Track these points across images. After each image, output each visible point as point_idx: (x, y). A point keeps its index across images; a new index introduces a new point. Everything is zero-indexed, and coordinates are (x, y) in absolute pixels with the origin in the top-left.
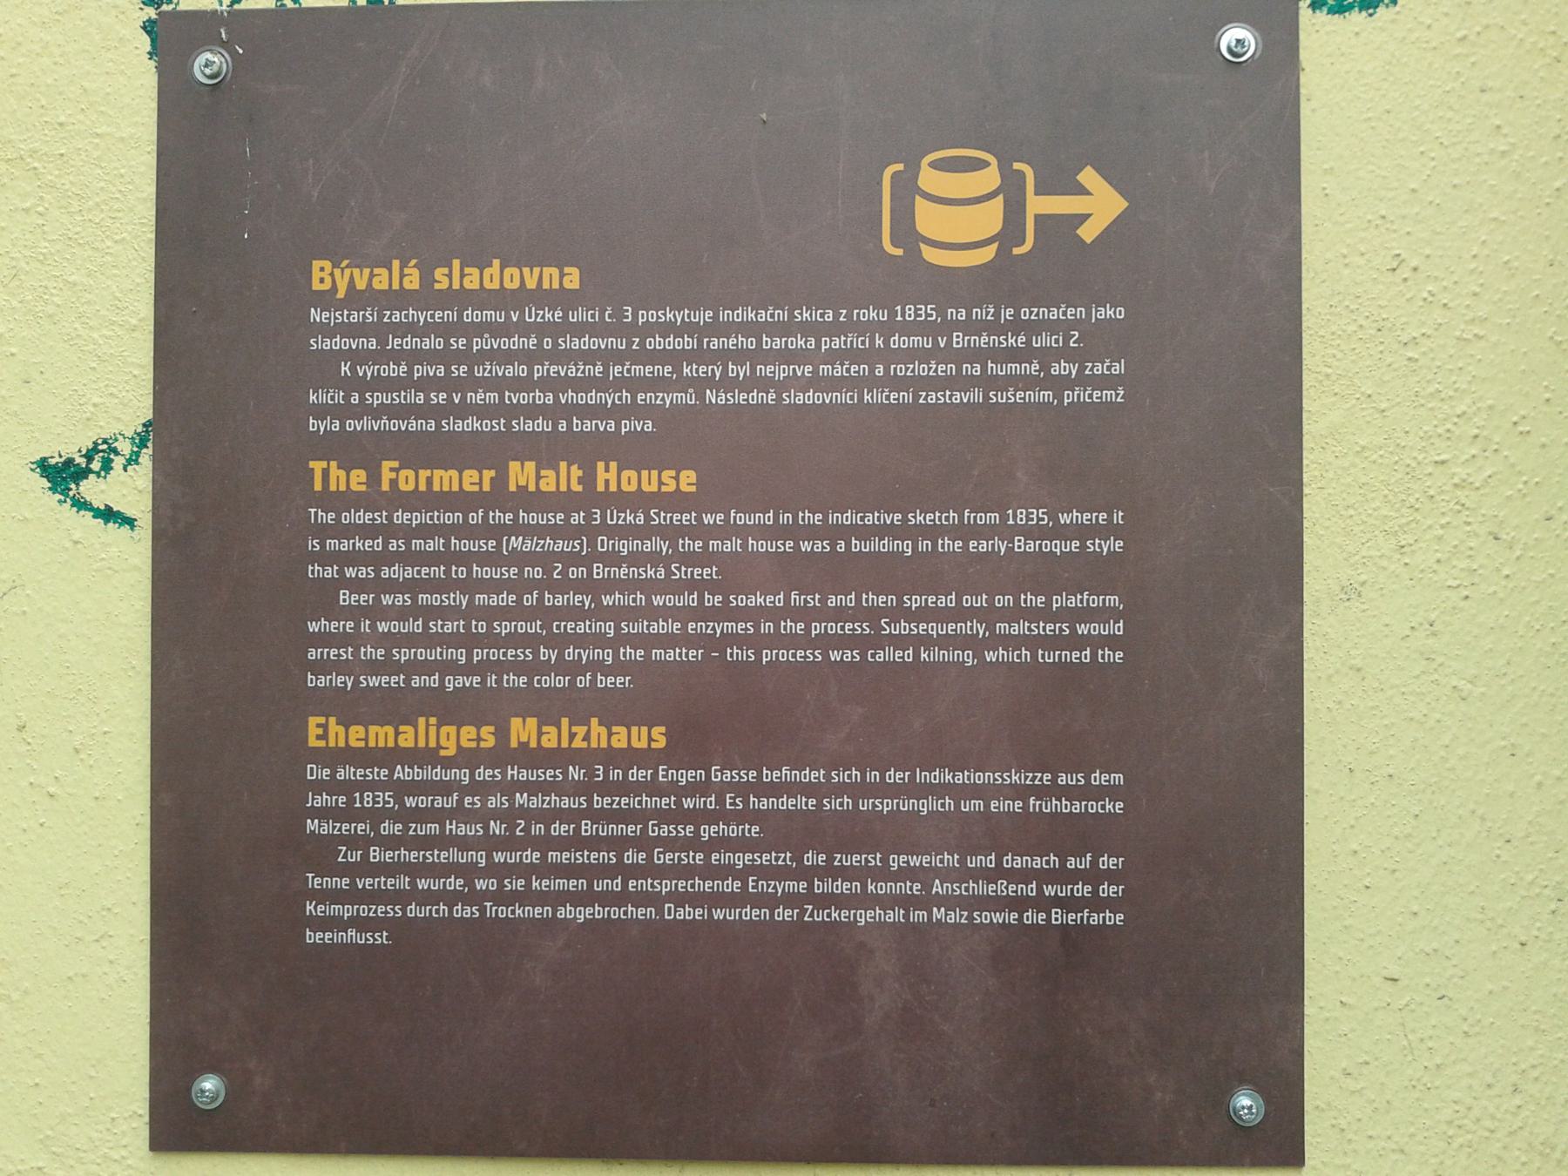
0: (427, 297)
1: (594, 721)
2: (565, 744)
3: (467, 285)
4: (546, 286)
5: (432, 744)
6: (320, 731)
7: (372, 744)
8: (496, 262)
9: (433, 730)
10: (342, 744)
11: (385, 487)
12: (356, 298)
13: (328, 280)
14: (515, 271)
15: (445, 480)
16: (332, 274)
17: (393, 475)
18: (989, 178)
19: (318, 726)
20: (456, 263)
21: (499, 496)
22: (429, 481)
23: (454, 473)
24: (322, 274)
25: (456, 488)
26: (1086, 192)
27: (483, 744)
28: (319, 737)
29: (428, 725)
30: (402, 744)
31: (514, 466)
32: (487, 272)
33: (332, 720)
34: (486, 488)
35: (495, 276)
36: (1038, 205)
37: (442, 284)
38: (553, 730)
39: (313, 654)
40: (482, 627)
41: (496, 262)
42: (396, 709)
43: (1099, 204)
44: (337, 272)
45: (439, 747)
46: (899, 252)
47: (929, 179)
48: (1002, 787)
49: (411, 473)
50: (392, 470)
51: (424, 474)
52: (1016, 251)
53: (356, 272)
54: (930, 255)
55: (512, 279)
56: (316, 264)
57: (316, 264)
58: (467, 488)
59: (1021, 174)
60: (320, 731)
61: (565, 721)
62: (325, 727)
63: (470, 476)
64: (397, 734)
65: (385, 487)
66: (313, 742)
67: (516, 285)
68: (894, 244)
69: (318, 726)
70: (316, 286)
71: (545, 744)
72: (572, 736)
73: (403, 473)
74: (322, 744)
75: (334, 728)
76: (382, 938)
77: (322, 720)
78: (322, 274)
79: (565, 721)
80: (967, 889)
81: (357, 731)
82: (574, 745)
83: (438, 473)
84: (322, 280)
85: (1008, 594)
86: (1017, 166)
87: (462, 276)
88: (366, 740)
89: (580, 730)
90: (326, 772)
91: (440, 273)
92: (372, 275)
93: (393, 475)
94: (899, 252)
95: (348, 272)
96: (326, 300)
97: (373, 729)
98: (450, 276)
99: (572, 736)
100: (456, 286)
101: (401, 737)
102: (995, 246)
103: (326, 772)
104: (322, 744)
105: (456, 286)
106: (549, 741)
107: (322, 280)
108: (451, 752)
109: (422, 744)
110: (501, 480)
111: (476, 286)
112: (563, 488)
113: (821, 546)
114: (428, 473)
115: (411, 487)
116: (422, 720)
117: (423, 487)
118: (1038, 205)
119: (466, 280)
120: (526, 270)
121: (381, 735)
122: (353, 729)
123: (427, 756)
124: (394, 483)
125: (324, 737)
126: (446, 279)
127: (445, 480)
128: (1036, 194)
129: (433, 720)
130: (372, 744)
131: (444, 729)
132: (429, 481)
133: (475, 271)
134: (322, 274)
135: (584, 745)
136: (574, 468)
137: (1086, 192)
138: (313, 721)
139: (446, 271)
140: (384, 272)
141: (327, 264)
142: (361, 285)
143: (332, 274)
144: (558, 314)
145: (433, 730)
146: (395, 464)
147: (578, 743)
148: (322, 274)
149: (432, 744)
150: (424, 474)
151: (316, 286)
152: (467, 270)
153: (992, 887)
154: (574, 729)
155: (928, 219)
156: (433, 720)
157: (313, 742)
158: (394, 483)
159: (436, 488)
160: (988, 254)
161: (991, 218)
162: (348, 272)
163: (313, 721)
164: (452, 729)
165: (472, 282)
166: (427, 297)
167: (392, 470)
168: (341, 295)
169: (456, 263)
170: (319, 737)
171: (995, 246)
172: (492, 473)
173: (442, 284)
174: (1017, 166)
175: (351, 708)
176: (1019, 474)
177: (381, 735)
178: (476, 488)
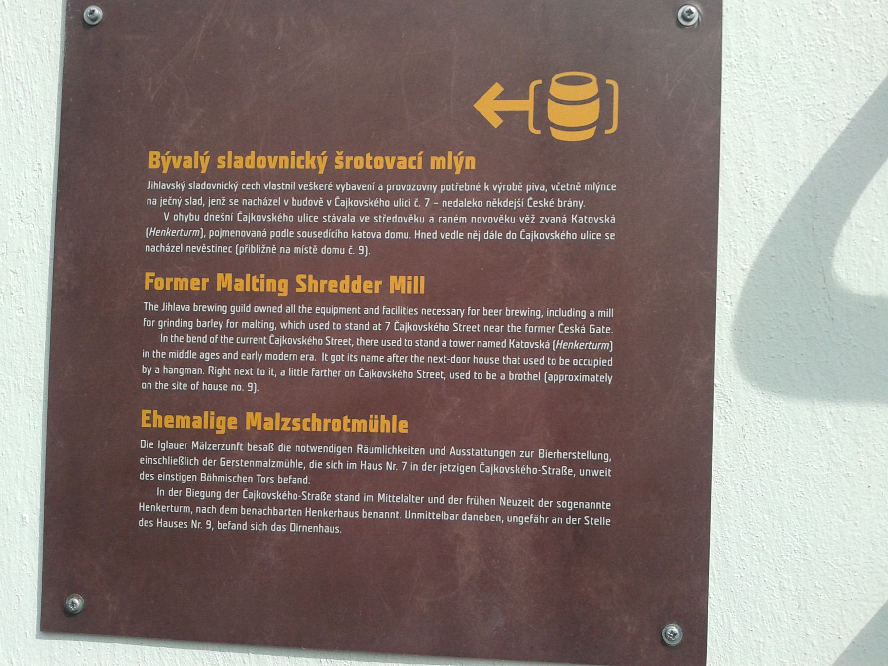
0: (214, 174)
1: (314, 415)
2: (277, 428)
3: (236, 166)
4: (281, 167)
5: (212, 427)
6: (148, 418)
7: (177, 426)
8: (253, 153)
9: (212, 419)
10: (160, 426)
11: (147, 287)
12: (174, 175)
13: (158, 163)
14: (263, 158)
15: (181, 283)
16: (160, 159)
17: (152, 281)
18: (592, 89)
19: (147, 415)
20: (230, 153)
21: (211, 295)
22: (172, 284)
23: (186, 280)
24: (155, 159)
25: (186, 288)
26: (500, 114)
27: (294, 429)
28: (147, 422)
29: (209, 416)
30: (195, 426)
31: (220, 276)
32: (248, 158)
33: (155, 412)
34: (204, 289)
35: (252, 161)
36: (527, 105)
37: (222, 165)
38: (270, 420)
39: (610, 362)
40: (350, 357)
41: (253, 153)
42: (192, 404)
43: (490, 106)
44: (163, 158)
45: (216, 429)
46: (538, 132)
47: (556, 89)
48: (551, 461)
49: (161, 280)
50: (151, 278)
51: (169, 280)
52: (607, 132)
53: (174, 158)
54: (556, 134)
55: (261, 162)
56: (152, 153)
57: (152, 153)
58: (193, 288)
59: (611, 86)
60: (148, 418)
61: (278, 415)
62: (151, 416)
63: (195, 281)
64: (192, 421)
65: (147, 287)
66: (144, 425)
67: (263, 166)
68: (536, 127)
69: (147, 415)
70: (151, 166)
71: (266, 428)
72: (282, 423)
73: (157, 279)
74: (149, 425)
75: (156, 416)
76: (336, 530)
77: (149, 412)
78: (155, 159)
79: (278, 415)
80: (161, 461)
81: (169, 419)
82: (282, 429)
83: (177, 280)
84: (155, 163)
85: (548, 345)
86: (608, 82)
87: (233, 160)
88: (174, 423)
89: (287, 420)
90: (151, 444)
91: (221, 159)
92: (183, 160)
93: (152, 281)
94: (538, 132)
95: (169, 158)
96: (158, 175)
97: (178, 417)
98: (226, 161)
99: (282, 423)
100: (230, 166)
101: (265, 424)
102: (595, 128)
103: (151, 444)
104: (149, 425)
105: (230, 166)
106: (269, 426)
107: (155, 163)
108: (223, 432)
109: (206, 427)
110: (212, 284)
111: (241, 167)
112: (248, 289)
113: (487, 312)
114: (171, 279)
115: (161, 288)
116: (206, 413)
117: (168, 288)
118: (527, 105)
119: (236, 163)
120: (270, 158)
121: (183, 422)
122: (167, 417)
123: (207, 435)
124: (152, 285)
125: (150, 421)
126: (224, 163)
127: (181, 283)
128: (527, 112)
129: (212, 413)
130: (177, 426)
131: (219, 419)
132: (172, 284)
133: (240, 158)
134: (155, 159)
135: (288, 429)
136: (254, 277)
137: (500, 114)
138: (145, 412)
139: (224, 158)
140: (190, 158)
141: (158, 154)
142: (176, 166)
143: (160, 159)
144: (520, 186)
145: (212, 419)
146: (153, 274)
147: (285, 428)
148: (155, 159)
149: (212, 427)
150: (169, 280)
151: (151, 166)
152: (236, 158)
153: (175, 460)
154: (283, 419)
155: (555, 112)
156: (212, 413)
157: (144, 425)
158: (152, 285)
159: (176, 288)
160: (590, 133)
161: (592, 112)
162: (169, 158)
163: (145, 412)
164: (223, 419)
165: (238, 165)
166: (214, 174)
167: (151, 278)
168: (165, 171)
169: (230, 153)
170: (147, 422)
171: (595, 128)
172: (208, 280)
173: (222, 165)
174: (608, 82)
175: (167, 403)
176: (554, 264)
177: (183, 422)
178: (198, 289)
